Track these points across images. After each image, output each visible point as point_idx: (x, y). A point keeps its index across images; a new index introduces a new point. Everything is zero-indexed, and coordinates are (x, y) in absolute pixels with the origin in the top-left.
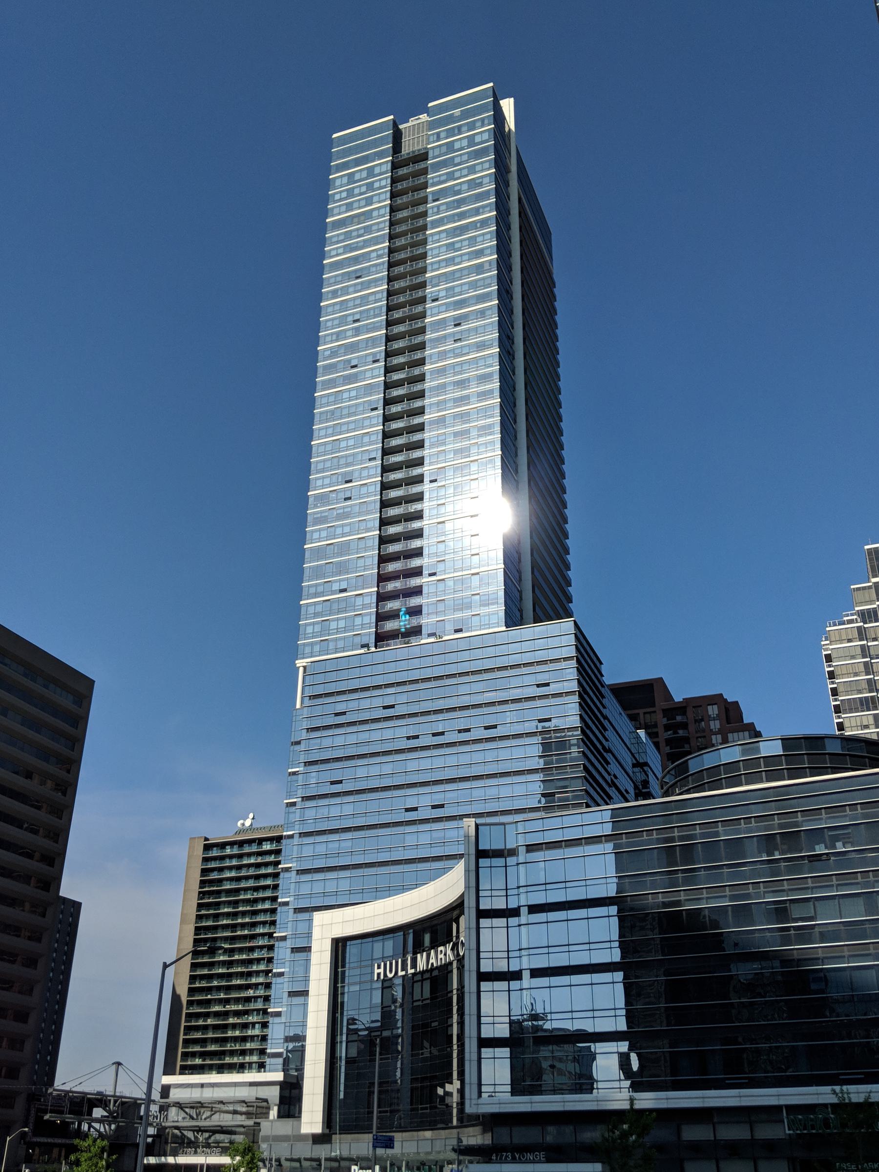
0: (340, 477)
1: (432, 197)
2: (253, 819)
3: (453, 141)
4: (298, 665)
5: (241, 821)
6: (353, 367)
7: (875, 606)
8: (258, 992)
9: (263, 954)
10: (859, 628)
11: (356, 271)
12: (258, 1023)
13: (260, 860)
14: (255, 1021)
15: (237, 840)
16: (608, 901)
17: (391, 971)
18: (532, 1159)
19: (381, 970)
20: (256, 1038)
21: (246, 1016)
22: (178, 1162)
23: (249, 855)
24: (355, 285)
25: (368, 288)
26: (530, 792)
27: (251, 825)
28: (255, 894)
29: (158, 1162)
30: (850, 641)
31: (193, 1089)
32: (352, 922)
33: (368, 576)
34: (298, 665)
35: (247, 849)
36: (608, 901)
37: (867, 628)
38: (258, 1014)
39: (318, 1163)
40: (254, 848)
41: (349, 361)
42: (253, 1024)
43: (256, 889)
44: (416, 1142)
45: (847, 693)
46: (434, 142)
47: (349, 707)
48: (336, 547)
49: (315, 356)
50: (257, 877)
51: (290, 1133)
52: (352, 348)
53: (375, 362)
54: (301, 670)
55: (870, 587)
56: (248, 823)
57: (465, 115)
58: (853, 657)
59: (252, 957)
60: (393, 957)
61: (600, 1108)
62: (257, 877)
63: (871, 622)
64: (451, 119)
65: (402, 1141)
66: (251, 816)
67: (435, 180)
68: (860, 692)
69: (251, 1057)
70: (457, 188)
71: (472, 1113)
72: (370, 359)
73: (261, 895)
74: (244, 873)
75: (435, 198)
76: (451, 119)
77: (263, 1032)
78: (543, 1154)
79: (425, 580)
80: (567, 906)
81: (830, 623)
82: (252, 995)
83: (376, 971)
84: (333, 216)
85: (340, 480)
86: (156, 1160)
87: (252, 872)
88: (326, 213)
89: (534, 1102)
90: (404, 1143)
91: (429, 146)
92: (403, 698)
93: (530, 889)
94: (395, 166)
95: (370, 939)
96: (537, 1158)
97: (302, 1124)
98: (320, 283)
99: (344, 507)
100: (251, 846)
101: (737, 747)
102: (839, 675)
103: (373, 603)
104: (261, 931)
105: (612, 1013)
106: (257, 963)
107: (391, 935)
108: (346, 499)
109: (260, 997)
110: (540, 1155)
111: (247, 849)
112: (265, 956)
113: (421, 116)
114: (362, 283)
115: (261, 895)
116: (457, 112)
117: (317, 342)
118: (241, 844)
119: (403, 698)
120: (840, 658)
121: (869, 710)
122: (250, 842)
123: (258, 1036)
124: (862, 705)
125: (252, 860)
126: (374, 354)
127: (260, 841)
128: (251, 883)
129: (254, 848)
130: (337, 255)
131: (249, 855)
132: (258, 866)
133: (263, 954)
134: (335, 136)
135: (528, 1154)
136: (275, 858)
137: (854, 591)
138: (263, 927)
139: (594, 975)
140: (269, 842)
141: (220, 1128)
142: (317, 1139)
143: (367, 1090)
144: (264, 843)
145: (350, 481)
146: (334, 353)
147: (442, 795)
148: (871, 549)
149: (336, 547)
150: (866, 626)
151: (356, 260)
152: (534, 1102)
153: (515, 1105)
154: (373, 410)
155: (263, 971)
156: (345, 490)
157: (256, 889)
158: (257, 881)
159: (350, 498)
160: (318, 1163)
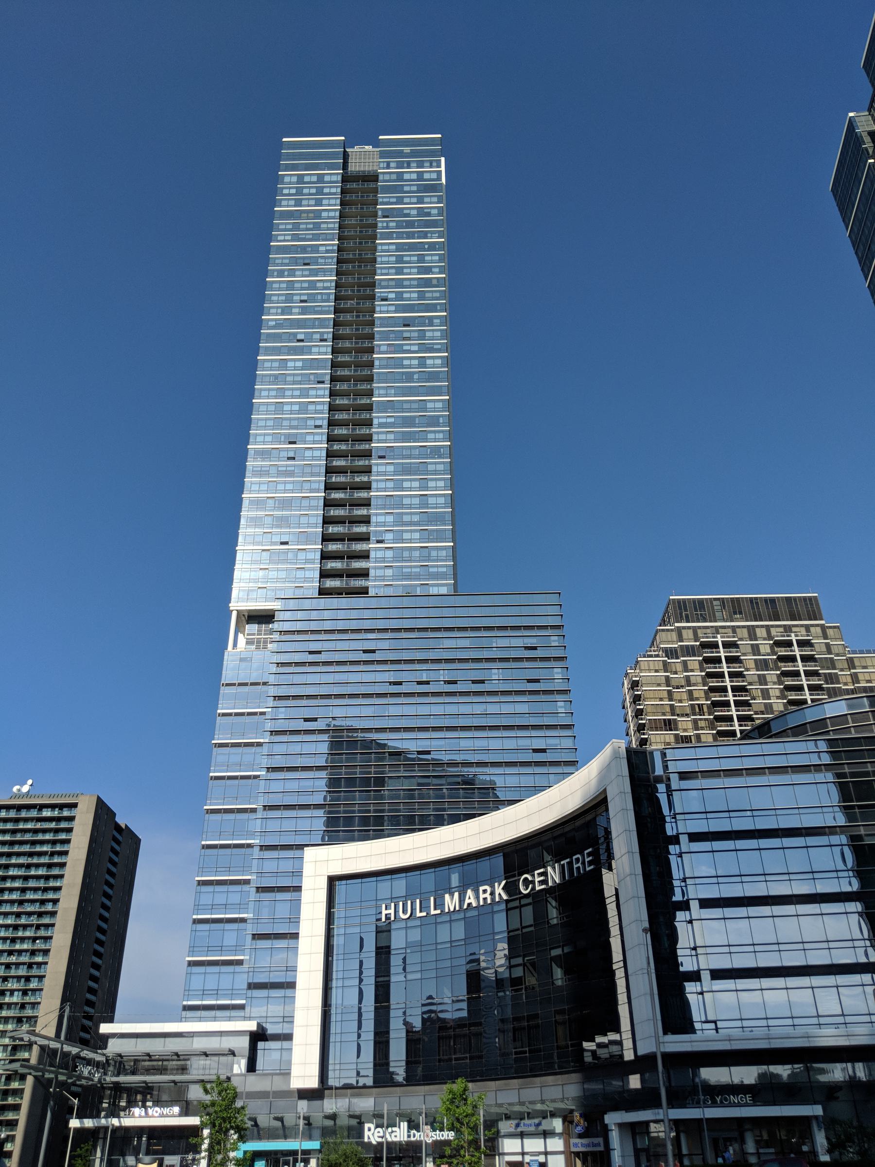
0: (283, 437)
1: (382, 213)
2: (31, 785)
3: (315, 206)
4: (231, 608)
5: (18, 787)
6: (299, 341)
7: (676, 646)
8: (21, 959)
9: (32, 921)
10: (663, 661)
11: (304, 258)
12: (18, 990)
13: (39, 826)
14: (15, 988)
15: (16, 804)
16: (803, 831)
17: (405, 912)
18: (736, 1102)
19: (392, 911)
20: (13, 1006)
21: (6, 983)
22: (123, 1125)
23: (26, 820)
24: (303, 270)
25: (316, 276)
26: (520, 746)
27: (29, 791)
28: (30, 859)
29: (96, 1125)
30: (656, 671)
31: (138, 1039)
32: (355, 859)
33: (311, 533)
34: (231, 608)
35: (24, 814)
36: (803, 831)
37: (670, 662)
38: (19, 981)
39: (359, 1120)
40: (34, 813)
41: (295, 334)
42: (12, 992)
43: (31, 854)
44: (540, 1088)
45: (654, 714)
46: (384, 168)
47: (324, 647)
48: (277, 502)
49: (259, 324)
50: (34, 843)
51: (268, 1089)
52: (300, 324)
53: (322, 340)
54: (234, 614)
55: (672, 630)
56: (25, 789)
57: (413, 154)
58: (659, 685)
59: (19, 923)
60: (405, 898)
61: (812, 1045)
62: (34, 843)
63: (672, 658)
64: (401, 154)
65: (424, 1096)
66: (30, 782)
67: (385, 200)
68: (664, 714)
69: (6, 1026)
70: (405, 212)
71: (648, 1053)
72: (318, 336)
73: (35, 860)
74: (19, 837)
75: (386, 214)
76: (401, 154)
77: (23, 1000)
78: (749, 1097)
79: (371, 546)
80: (756, 834)
81: (640, 655)
82: (14, 961)
83: (384, 912)
84: (280, 206)
85: (282, 440)
86: (94, 1123)
87: (28, 837)
88: (275, 203)
89: (667, 1042)
90: (520, 1090)
91: (379, 171)
92: (385, 645)
93: (687, 817)
94: (345, 179)
95: (374, 879)
96: (743, 1101)
97: (292, 1078)
98: (267, 262)
99: (287, 466)
100: (9, 811)
101: (844, 701)
102: (647, 698)
103: (317, 559)
104: (32, 897)
105: (850, 944)
106: (24, 929)
107: (404, 875)
108: (289, 458)
109: (24, 964)
110: (746, 1098)
111: (24, 814)
112: (35, 922)
113: (366, 147)
114: (310, 270)
115: (35, 860)
116: (407, 150)
117: (261, 311)
118: (19, 808)
119: (385, 645)
120: (648, 684)
121: (671, 730)
122: (29, 807)
123: (16, 1004)
124: (665, 725)
125: (29, 826)
126: (322, 334)
127: (42, 807)
128: (26, 848)
129: (34, 813)
130: (284, 241)
131: (26, 820)
132: (36, 831)
133: (32, 921)
134: (284, 140)
135: (732, 1097)
136: (56, 825)
137: (219, 716)
138: (34, 893)
139: (750, 909)
140: (50, 809)
141: (144, 1085)
142: (304, 1094)
143: (437, 1034)
144: (43, 810)
145: (294, 443)
146: (279, 325)
147: (428, 742)
148: (675, 599)
149: (277, 502)
150: (669, 661)
151: (304, 249)
152: (667, 1042)
153: (710, 1043)
154: (319, 382)
155: (29, 938)
156: (287, 450)
157: (31, 854)
158: (34, 847)
159: (294, 458)
160: (359, 1120)
